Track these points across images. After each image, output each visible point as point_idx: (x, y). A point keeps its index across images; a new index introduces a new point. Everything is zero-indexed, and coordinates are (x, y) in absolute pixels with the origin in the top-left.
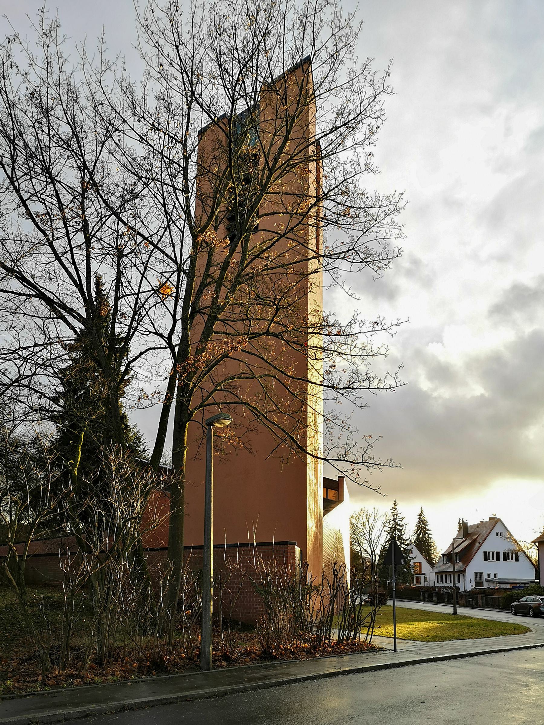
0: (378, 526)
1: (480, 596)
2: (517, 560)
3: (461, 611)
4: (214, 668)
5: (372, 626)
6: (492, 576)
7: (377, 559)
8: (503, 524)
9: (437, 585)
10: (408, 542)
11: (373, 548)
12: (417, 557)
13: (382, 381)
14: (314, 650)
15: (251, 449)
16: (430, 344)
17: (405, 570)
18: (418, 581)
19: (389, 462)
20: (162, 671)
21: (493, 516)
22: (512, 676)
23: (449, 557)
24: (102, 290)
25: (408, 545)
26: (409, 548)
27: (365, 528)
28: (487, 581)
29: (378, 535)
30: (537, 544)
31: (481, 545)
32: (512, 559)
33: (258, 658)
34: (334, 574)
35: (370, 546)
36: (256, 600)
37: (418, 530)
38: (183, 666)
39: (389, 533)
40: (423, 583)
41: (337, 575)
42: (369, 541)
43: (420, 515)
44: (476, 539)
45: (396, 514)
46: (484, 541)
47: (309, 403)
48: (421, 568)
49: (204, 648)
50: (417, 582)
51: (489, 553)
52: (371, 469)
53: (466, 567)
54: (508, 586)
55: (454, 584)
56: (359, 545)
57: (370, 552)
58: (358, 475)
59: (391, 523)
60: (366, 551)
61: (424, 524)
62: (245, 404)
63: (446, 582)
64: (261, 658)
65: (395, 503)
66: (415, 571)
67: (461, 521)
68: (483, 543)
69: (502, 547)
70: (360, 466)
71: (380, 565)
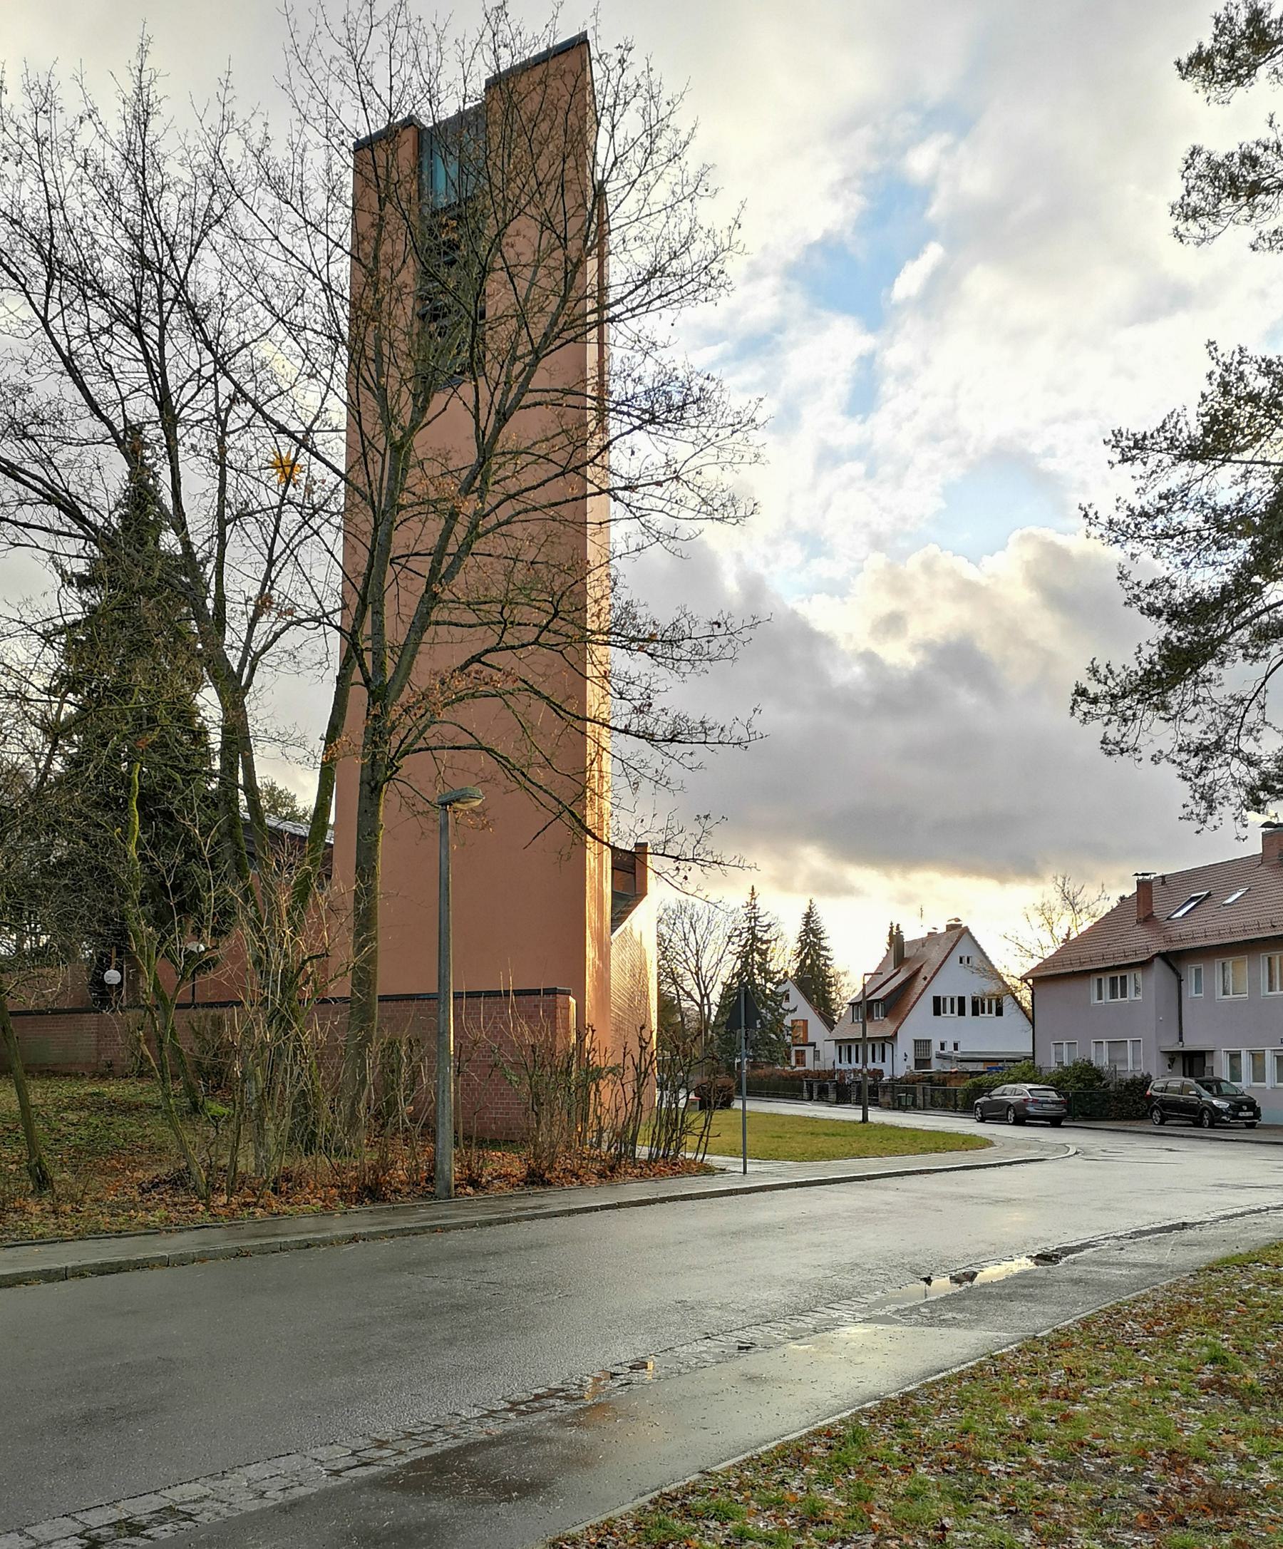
0: (719, 935)
1: (919, 1087)
2: (999, 1012)
3: (876, 1116)
4: (456, 1197)
5: (705, 1133)
6: (949, 1048)
7: (714, 1013)
8: (973, 938)
9: (838, 1066)
10: (780, 976)
11: (706, 988)
12: (799, 1008)
13: (727, 732)
14: (611, 1172)
16: (824, 594)
17: (773, 1036)
18: (801, 1061)
19: (737, 859)
20: (378, 1199)
21: (953, 922)
22: (924, 1201)
23: (865, 1007)
24: (145, 457)
25: (778, 984)
26: (781, 989)
27: (687, 945)
28: (939, 1056)
29: (714, 960)
30: (1030, 981)
31: (929, 982)
32: (990, 1012)
33: (521, 1184)
34: (641, 1047)
35: (698, 985)
36: (496, 1094)
37: (803, 949)
38: (409, 1193)
39: (738, 958)
40: (810, 1065)
41: (645, 1048)
42: (697, 974)
43: (808, 916)
44: (919, 970)
46: (935, 974)
47: (649, 864)
48: (806, 1032)
49: (442, 1164)
50: (797, 1062)
51: (945, 999)
52: (707, 870)
53: (898, 1028)
54: (980, 1067)
55: (865, 1062)
56: (675, 982)
57: (698, 998)
58: (686, 878)
59: (744, 935)
60: (689, 994)
61: (815, 936)
62: (487, 750)
64: (526, 1183)
65: (753, 894)
66: (794, 1038)
67: (894, 929)
68: (932, 978)
69: (971, 987)
70: (690, 864)
71: (719, 1026)
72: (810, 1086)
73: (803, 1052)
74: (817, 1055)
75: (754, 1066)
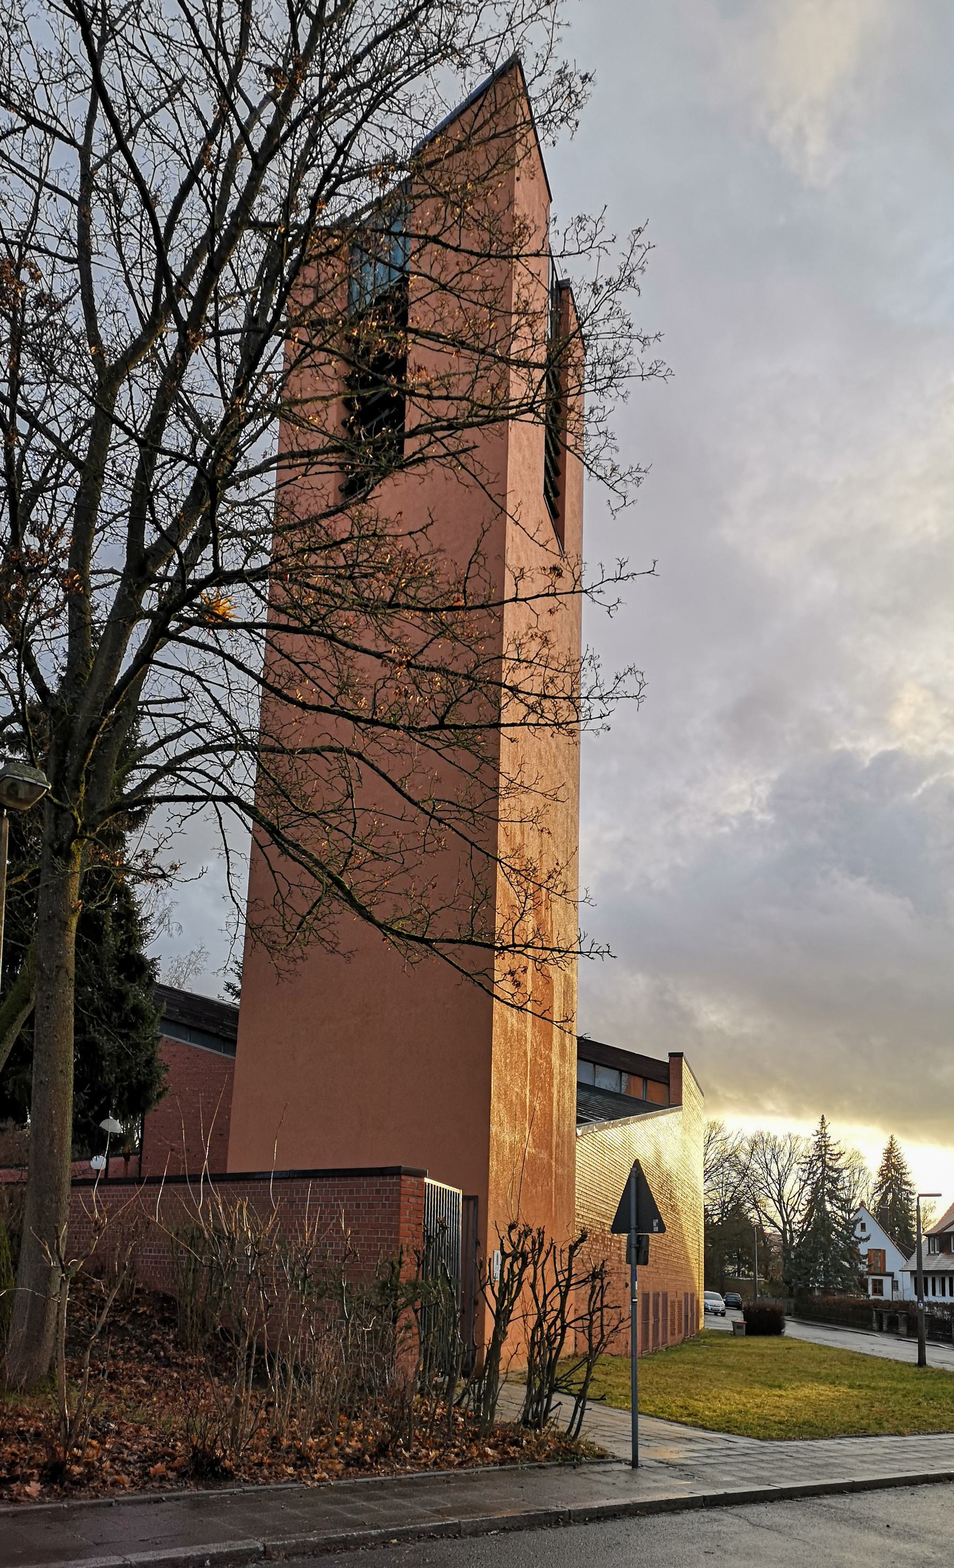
11: (788, 1216)
15: (337, 944)
18: (878, 1289)
33: (171, 1475)
35: (781, 1213)
40: (888, 1294)
42: (779, 1202)
45: (826, 1146)
57: (781, 1225)
60: (772, 1221)
61: (897, 1170)
63: (934, 1294)
72: (880, 1316)
73: (881, 1282)
74: (895, 1285)
75: (825, 1292)
